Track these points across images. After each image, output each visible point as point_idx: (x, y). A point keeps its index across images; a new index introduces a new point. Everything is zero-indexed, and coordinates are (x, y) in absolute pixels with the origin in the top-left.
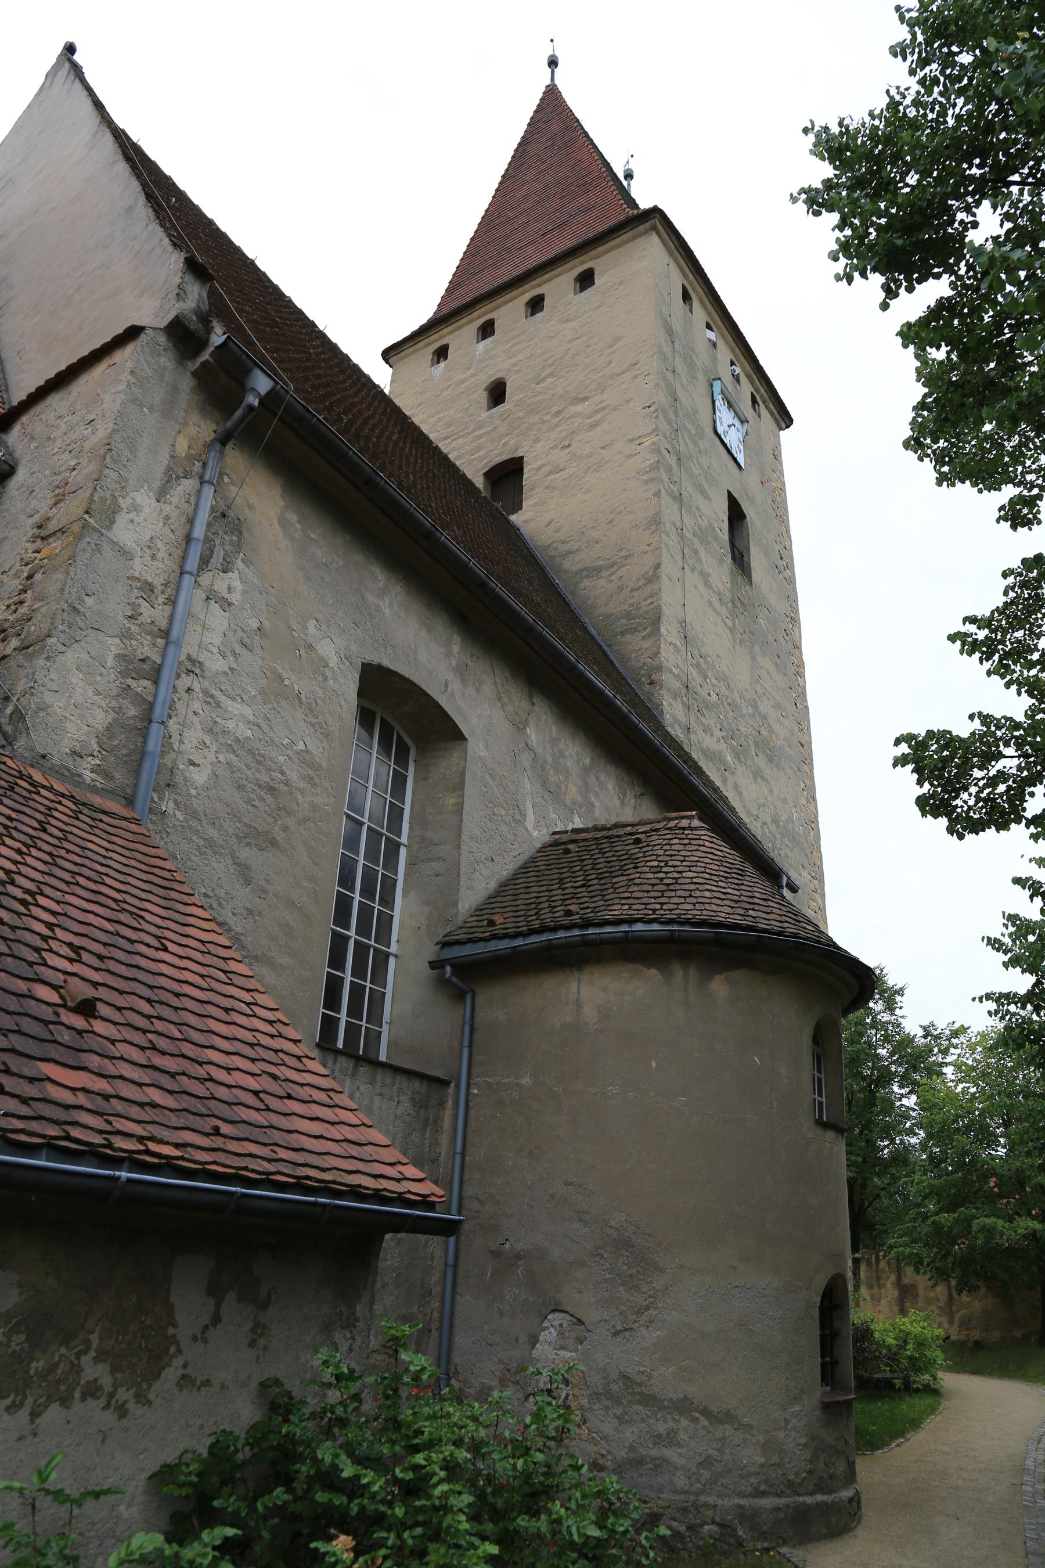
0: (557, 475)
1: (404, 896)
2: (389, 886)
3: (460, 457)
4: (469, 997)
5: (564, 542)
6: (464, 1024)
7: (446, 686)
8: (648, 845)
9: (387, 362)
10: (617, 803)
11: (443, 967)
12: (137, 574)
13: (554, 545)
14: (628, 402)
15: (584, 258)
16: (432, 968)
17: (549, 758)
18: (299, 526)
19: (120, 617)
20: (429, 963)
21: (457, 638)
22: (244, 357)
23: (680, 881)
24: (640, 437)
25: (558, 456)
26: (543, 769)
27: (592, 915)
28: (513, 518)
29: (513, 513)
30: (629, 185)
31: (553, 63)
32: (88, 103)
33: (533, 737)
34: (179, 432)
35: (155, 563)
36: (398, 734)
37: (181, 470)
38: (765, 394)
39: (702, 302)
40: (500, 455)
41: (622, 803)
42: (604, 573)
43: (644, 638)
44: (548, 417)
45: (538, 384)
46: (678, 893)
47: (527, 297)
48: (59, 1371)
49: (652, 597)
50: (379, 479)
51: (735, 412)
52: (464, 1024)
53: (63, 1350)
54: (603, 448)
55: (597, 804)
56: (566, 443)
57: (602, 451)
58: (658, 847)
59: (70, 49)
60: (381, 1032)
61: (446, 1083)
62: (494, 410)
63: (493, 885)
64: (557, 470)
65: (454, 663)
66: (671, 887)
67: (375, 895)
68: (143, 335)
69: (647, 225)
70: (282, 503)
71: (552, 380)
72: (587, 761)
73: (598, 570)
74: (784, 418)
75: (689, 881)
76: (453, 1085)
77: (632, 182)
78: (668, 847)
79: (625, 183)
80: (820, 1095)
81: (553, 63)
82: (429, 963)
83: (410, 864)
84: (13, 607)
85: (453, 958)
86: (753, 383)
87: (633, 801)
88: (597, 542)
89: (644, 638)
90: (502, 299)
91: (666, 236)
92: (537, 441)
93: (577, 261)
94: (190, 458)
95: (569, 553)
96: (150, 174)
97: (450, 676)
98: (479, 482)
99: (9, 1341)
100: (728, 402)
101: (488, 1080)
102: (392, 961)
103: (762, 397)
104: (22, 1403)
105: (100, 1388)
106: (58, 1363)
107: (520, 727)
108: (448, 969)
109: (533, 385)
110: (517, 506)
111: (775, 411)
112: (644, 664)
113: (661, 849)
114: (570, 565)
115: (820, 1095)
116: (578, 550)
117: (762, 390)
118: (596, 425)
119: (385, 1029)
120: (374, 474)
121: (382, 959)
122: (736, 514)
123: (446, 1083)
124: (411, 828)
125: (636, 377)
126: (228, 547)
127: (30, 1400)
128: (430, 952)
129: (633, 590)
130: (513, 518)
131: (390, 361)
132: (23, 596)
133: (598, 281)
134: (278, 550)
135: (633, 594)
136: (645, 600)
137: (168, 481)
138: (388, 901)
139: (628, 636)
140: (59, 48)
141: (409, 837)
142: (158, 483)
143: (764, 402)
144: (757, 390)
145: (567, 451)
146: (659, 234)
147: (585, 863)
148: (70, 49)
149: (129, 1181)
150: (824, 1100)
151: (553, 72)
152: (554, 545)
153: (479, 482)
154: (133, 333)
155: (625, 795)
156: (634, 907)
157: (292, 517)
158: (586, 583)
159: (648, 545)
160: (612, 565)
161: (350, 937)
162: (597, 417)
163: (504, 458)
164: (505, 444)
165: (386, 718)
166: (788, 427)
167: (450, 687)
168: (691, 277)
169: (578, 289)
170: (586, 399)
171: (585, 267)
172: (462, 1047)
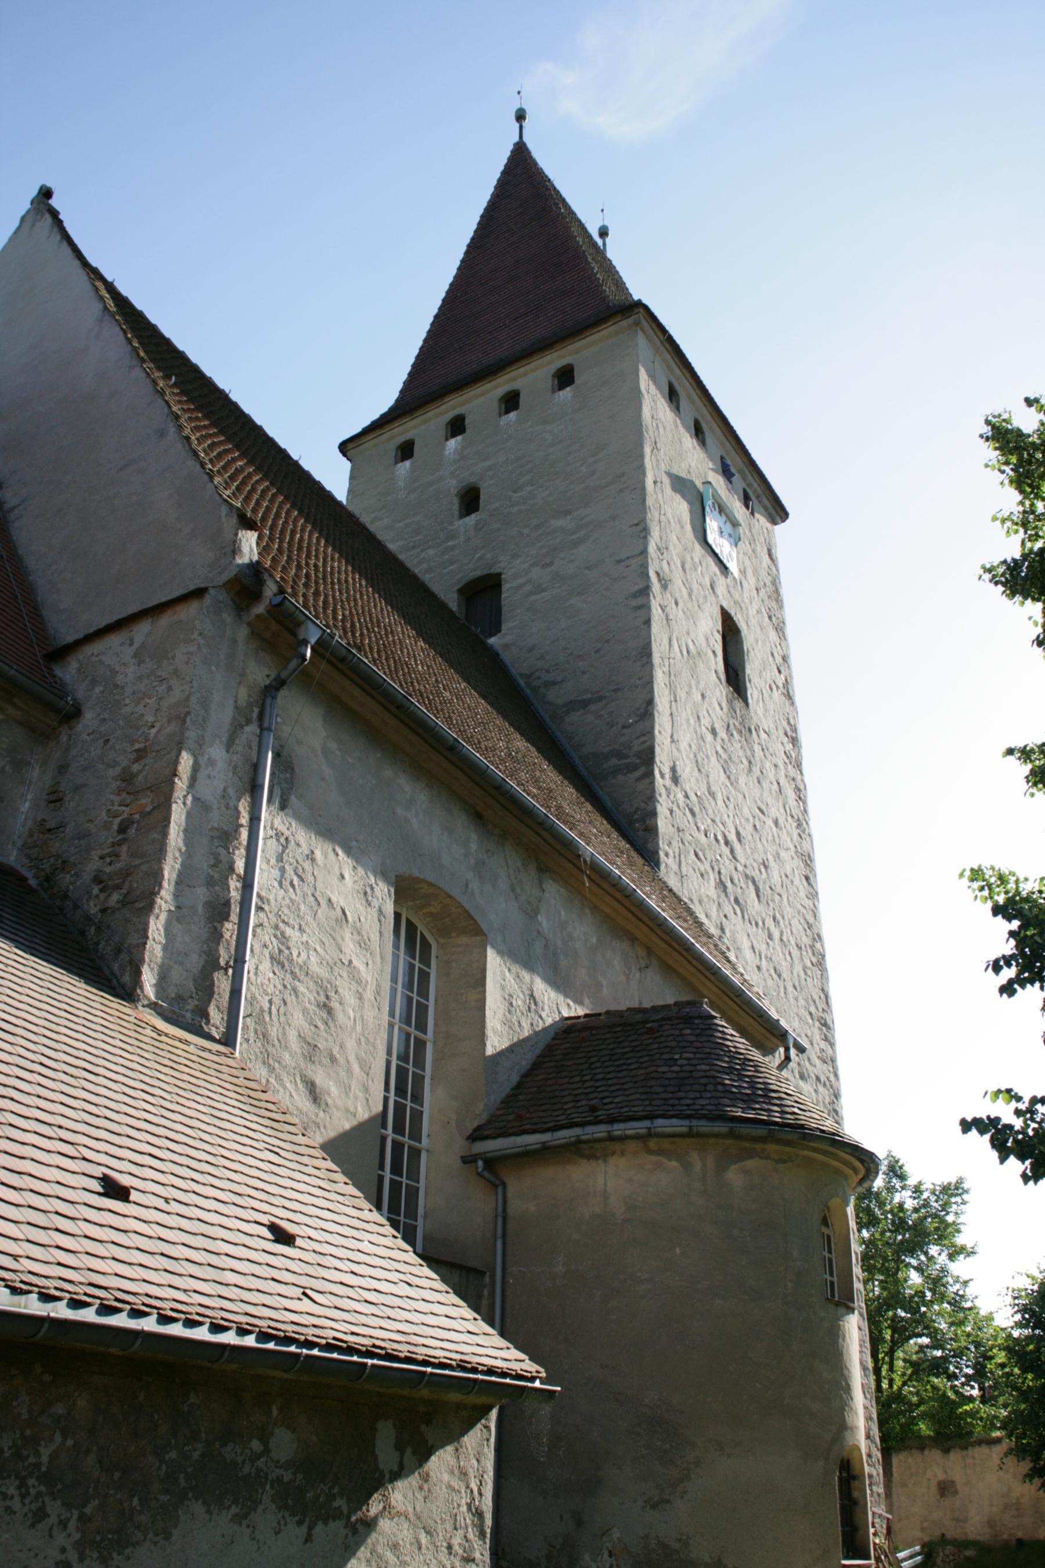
0: (538, 596)
1: (432, 1091)
2: (419, 1080)
3: (429, 570)
4: (500, 1189)
5: (547, 671)
6: (496, 1217)
7: (467, 886)
8: (661, 1036)
9: (344, 454)
10: (623, 978)
11: (475, 1161)
12: (216, 825)
13: (538, 674)
14: (614, 518)
15: (562, 352)
16: (465, 1162)
17: (559, 943)
18: (338, 753)
19: (205, 867)
20: (462, 1157)
21: (474, 837)
22: (297, 612)
23: (695, 1074)
24: (628, 558)
25: (536, 573)
26: (555, 954)
27: (616, 1111)
28: (492, 641)
29: (491, 635)
30: (604, 244)
31: (520, 116)
32: (81, 276)
33: (545, 923)
34: (240, 683)
35: (228, 812)
36: (421, 932)
37: (244, 719)
38: (759, 489)
39: (689, 397)
40: (471, 569)
41: (628, 978)
42: (593, 707)
43: (637, 780)
44: (526, 531)
45: (515, 492)
46: (695, 1087)
47: (501, 391)
48: (321, 1500)
49: (644, 735)
50: (409, 704)
51: (727, 516)
52: (496, 1217)
53: (322, 1485)
54: (588, 568)
55: (604, 983)
56: (548, 560)
57: (587, 572)
58: (671, 1038)
59: (46, 193)
60: (416, 1227)
61: (483, 1273)
62: (467, 519)
63: (515, 1078)
64: (540, 589)
65: (472, 861)
66: (687, 1081)
67: (406, 1092)
68: (207, 596)
69: (631, 320)
70: (324, 734)
71: (530, 488)
72: (594, 940)
73: (584, 704)
74: (778, 512)
75: (703, 1074)
76: (488, 1274)
77: (608, 240)
78: (680, 1039)
79: (600, 242)
80: (831, 1275)
81: (520, 116)
82: (462, 1157)
83: (436, 1060)
84: (108, 860)
85: (485, 1153)
86: (744, 479)
87: (638, 975)
88: (584, 673)
89: (637, 780)
90: (473, 393)
91: (650, 331)
92: (515, 556)
93: (555, 355)
94: (250, 705)
95: (553, 683)
96: (113, 298)
97: (469, 875)
98: (452, 601)
99: (295, 1478)
100: (720, 506)
101: (522, 1269)
102: (424, 1156)
103: (755, 491)
104: (304, 1521)
105: (342, 1513)
106: (320, 1495)
107: (531, 913)
108: (480, 1163)
109: (510, 493)
110: (495, 628)
111: (769, 506)
112: (637, 809)
113: (674, 1040)
114: (554, 696)
115: (831, 1275)
116: (563, 681)
117: (755, 485)
118: (580, 542)
119: (420, 1221)
120: (405, 700)
121: (415, 1153)
122: (730, 631)
123: (483, 1273)
124: (436, 1025)
125: (621, 491)
126: (284, 786)
127: (307, 1520)
128: (460, 1146)
129: (624, 727)
130: (492, 641)
131: (349, 454)
132: (117, 848)
133: (579, 379)
134: (323, 779)
135: (624, 731)
136: (638, 738)
137: (234, 732)
138: (417, 1098)
139: (620, 777)
140: (34, 192)
141: (435, 1032)
142: (226, 735)
143: (758, 497)
144: (749, 485)
145: (549, 570)
146: (643, 330)
147: (602, 1053)
148: (46, 193)
149: (432, 1374)
150: (835, 1279)
151: (521, 128)
152: (538, 674)
153: (452, 601)
154: (199, 593)
155: (630, 969)
156: (654, 1103)
157: (333, 745)
158: (575, 717)
159: (640, 679)
160: (601, 699)
161: (388, 1135)
162: (582, 533)
163: (478, 573)
164: (481, 558)
165: (410, 918)
166: (783, 521)
167: (470, 886)
168: (678, 371)
169: (556, 387)
170: (569, 512)
171: (564, 362)
172: (495, 1238)
